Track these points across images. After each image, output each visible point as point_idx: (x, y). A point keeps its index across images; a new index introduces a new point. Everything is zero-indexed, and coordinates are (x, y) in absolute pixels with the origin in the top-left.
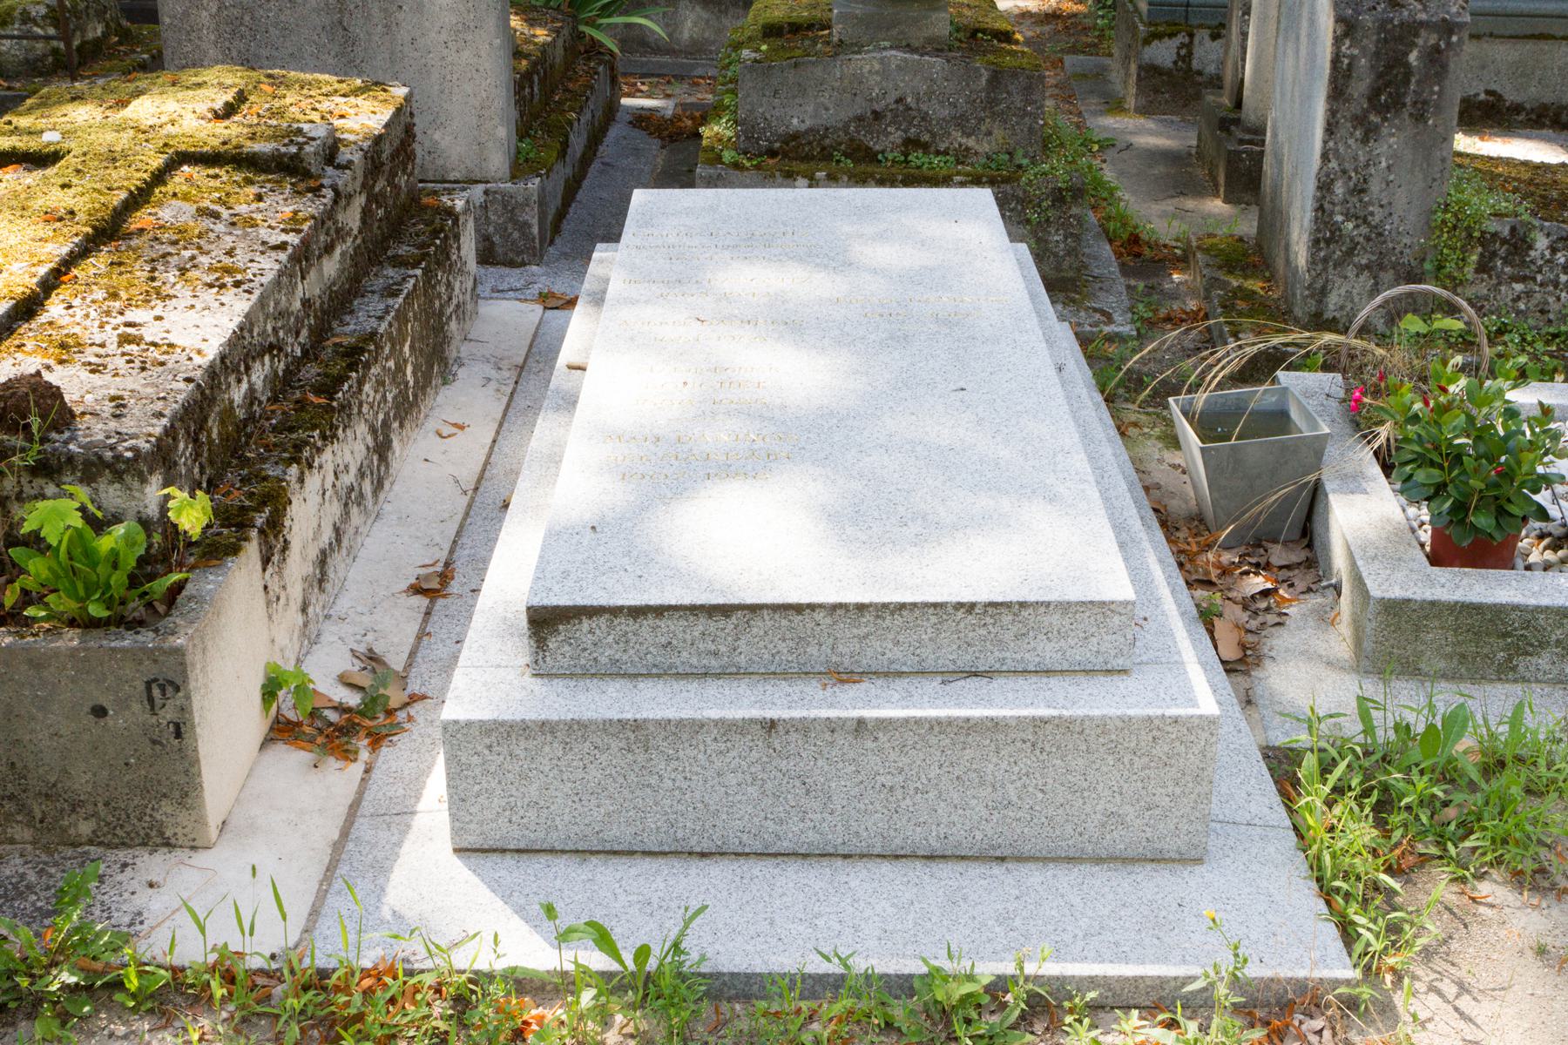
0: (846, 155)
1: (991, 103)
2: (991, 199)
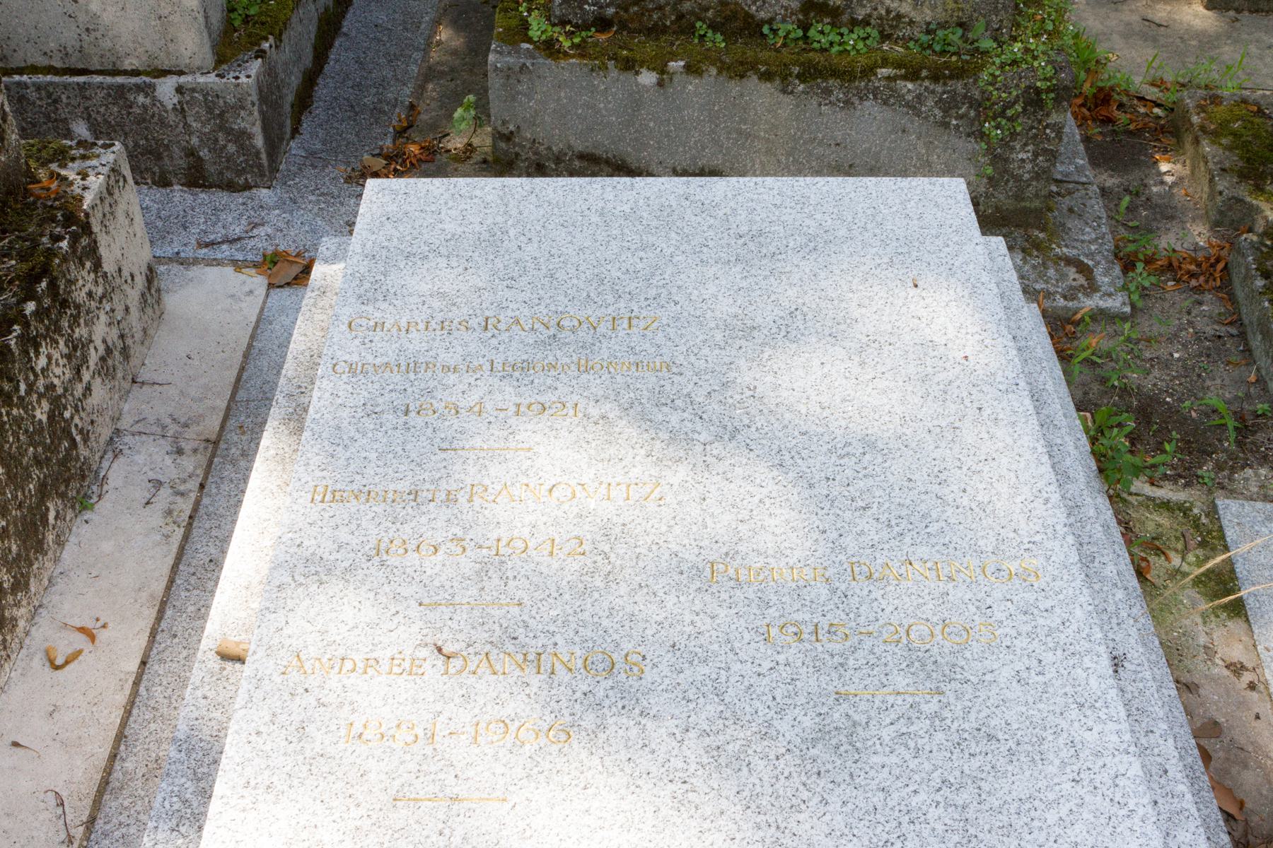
0: (714, 27)
2: (964, 187)
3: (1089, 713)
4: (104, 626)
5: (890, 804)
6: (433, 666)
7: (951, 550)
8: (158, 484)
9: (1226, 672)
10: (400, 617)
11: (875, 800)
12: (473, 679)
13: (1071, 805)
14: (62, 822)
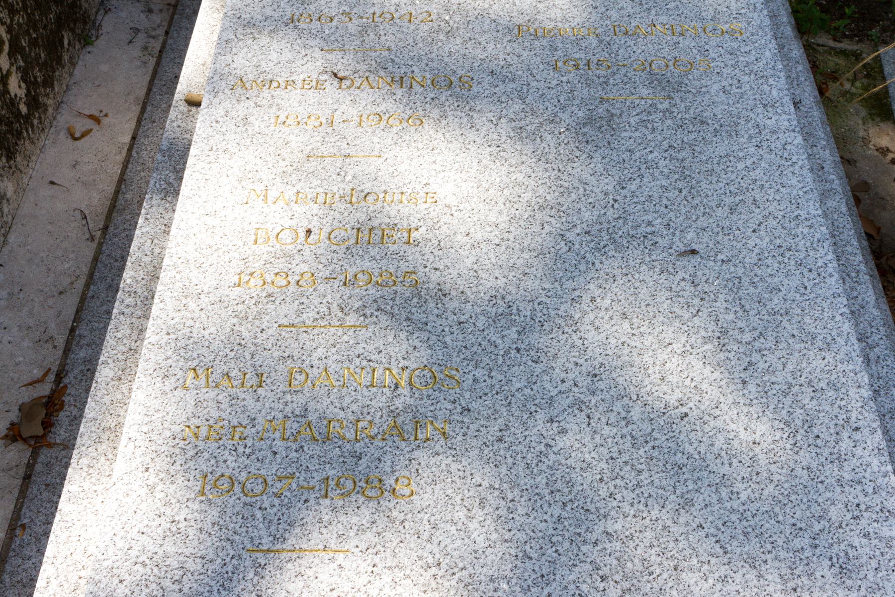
3: (770, 109)
4: (106, 115)
5: (634, 158)
6: (331, 86)
7: (683, 18)
8: (137, 31)
9: (876, 153)
10: (309, 57)
11: (624, 156)
12: (358, 91)
13: (755, 159)
14: (86, 228)
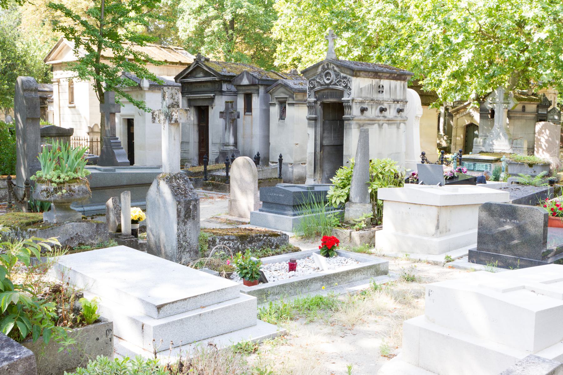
1: (97, 231)
